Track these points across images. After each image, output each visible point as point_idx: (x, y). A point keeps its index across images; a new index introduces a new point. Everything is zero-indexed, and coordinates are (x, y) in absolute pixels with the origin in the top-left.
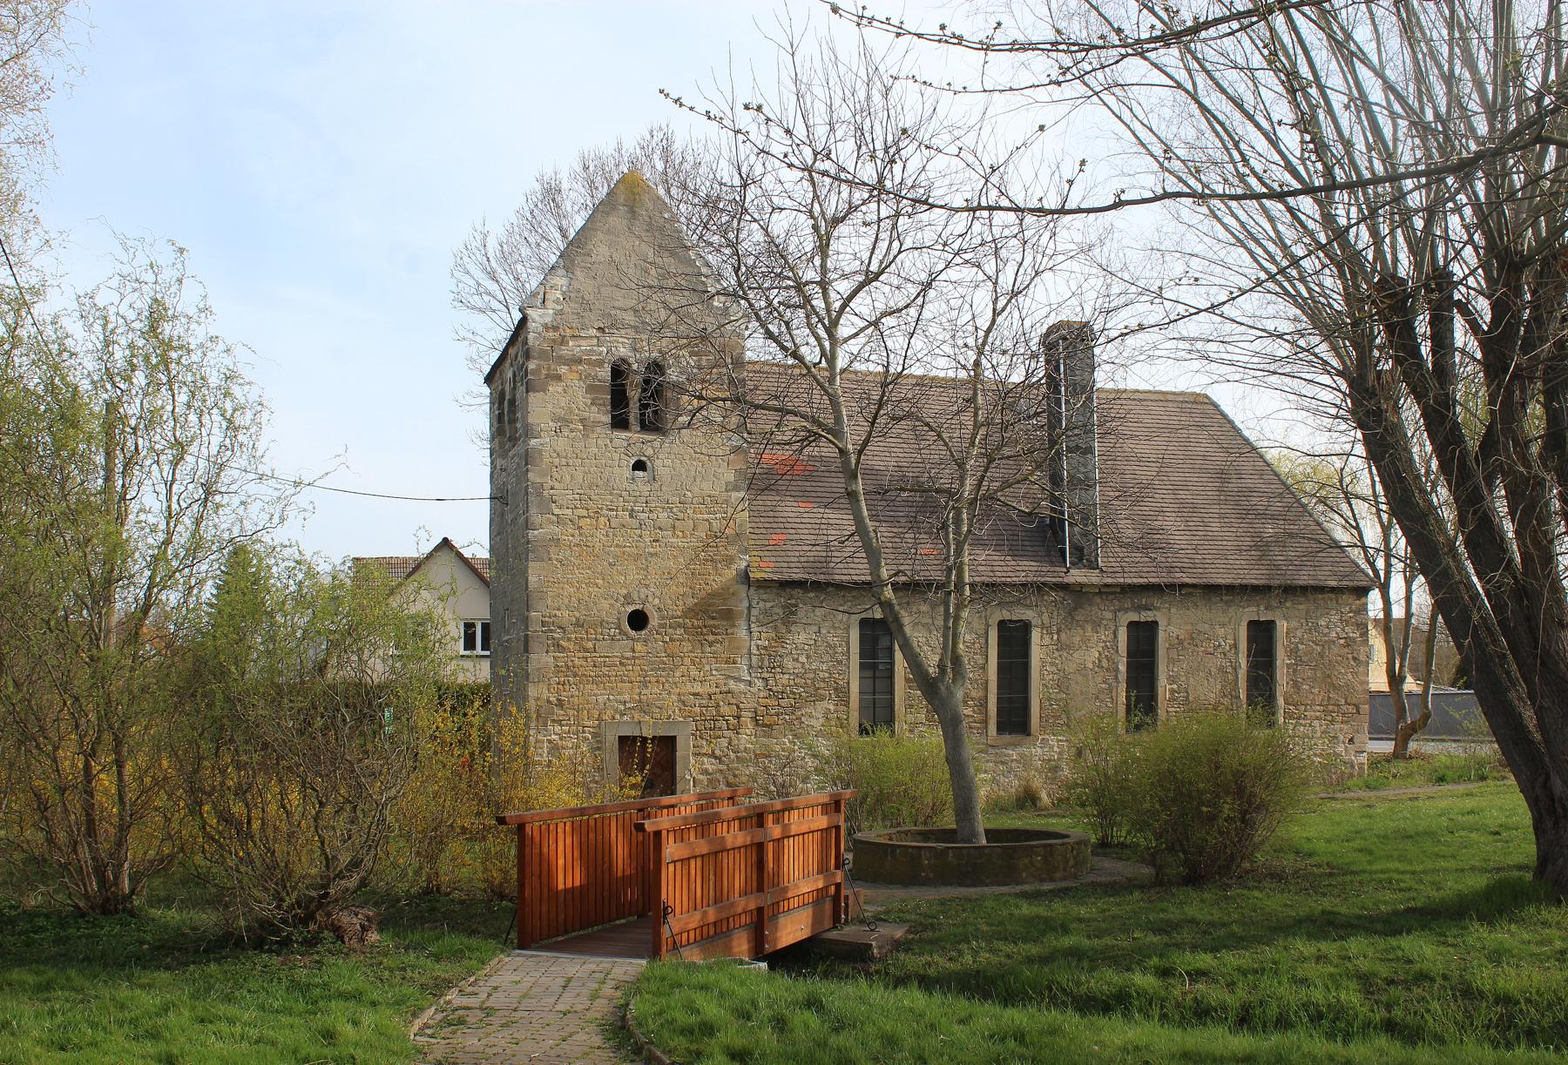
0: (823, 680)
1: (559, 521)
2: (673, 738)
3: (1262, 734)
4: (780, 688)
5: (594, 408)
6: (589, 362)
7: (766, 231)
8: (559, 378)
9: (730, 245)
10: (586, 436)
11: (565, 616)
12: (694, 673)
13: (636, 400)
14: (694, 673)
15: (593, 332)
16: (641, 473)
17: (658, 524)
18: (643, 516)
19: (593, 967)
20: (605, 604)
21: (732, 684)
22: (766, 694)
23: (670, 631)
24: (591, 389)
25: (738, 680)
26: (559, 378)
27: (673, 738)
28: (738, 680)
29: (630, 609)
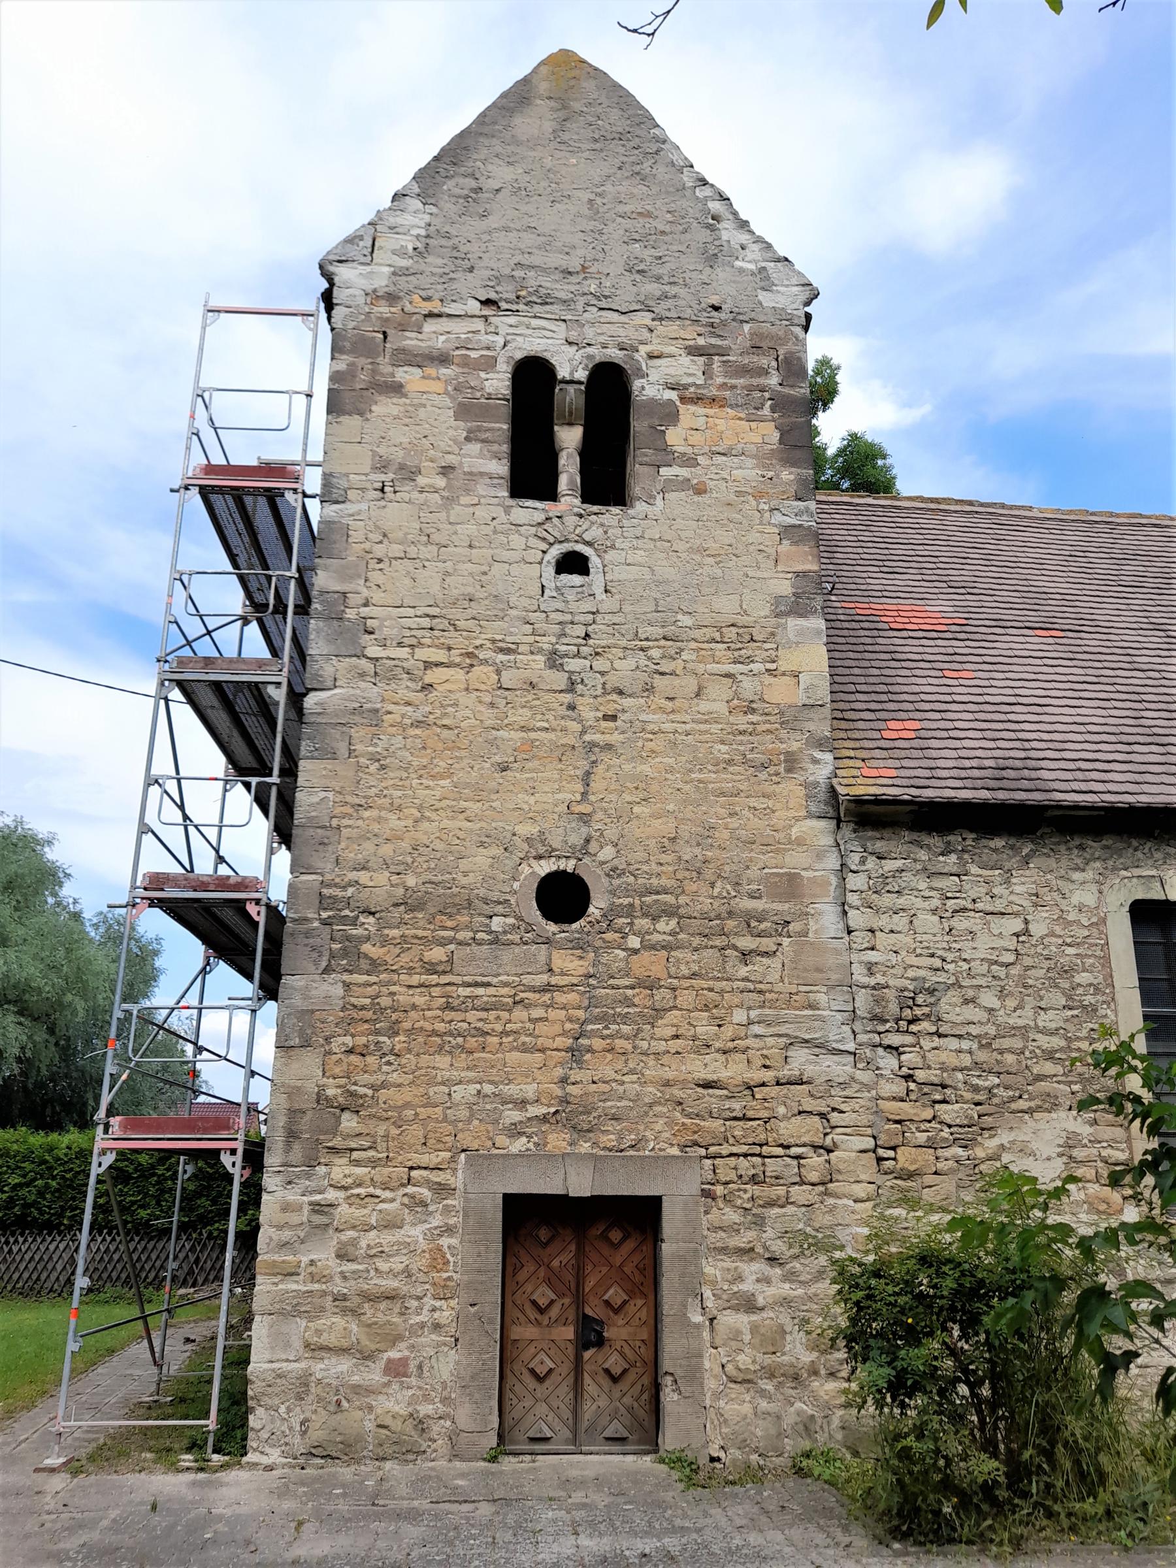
0: (1050, 1055)
1: (381, 672)
2: (655, 1203)
3: (543, 87)
4: (933, 1075)
5: (475, 448)
6: (466, 362)
7: (217, 851)
8: (397, 389)
9: (802, 1252)
10: (450, 501)
11: (378, 885)
12: (704, 1030)
13: (573, 435)
14: (704, 1030)
15: (474, 307)
16: (576, 579)
17: (613, 680)
18: (573, 664)
19: (667, 683)
20: (481, 860)
21: (801, 1061)
22: (899, 1088)
23: (643, 923)
24: (464, 411)
25: (821, 1047)
26: (397, 389)
27: (655, 1203)
28: (821, 1047)
29: (545, 868)
